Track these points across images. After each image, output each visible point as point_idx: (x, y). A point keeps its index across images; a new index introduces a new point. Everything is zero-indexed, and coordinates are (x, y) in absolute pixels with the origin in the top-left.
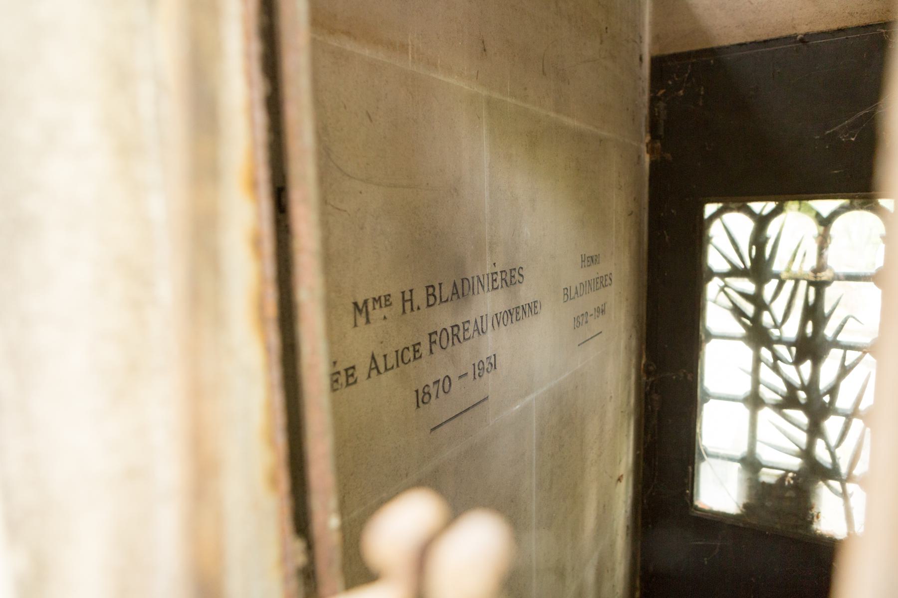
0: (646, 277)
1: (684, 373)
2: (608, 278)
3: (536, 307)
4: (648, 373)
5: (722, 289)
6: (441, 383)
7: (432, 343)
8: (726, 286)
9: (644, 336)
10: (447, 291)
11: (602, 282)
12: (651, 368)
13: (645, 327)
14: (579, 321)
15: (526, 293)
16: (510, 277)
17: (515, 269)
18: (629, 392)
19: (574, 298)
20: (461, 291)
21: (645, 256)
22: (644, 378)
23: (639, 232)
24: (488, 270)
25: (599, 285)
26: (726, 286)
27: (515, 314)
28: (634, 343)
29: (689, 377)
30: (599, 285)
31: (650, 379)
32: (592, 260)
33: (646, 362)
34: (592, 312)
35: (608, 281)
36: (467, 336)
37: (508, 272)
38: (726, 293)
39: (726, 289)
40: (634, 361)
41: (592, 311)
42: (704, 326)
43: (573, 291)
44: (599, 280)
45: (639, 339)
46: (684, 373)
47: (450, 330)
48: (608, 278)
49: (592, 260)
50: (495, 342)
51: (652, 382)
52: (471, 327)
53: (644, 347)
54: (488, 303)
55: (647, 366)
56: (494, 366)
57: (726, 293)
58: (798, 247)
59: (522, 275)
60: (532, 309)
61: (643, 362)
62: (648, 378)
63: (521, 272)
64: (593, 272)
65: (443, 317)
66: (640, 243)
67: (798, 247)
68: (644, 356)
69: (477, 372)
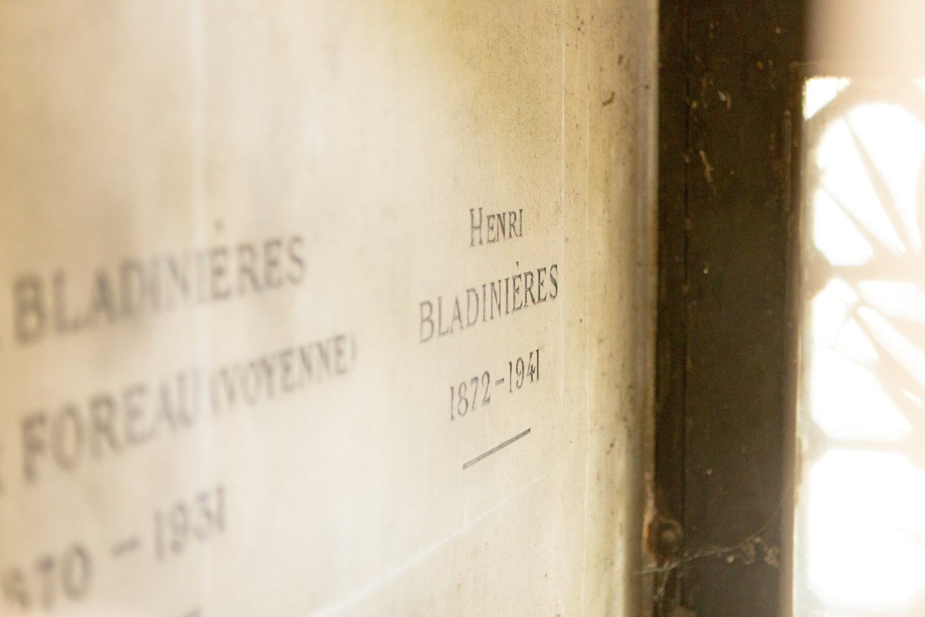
0: (652, 280)
1: (758, 547)
2: (545, 277)
3: (339, 352)
4: (661, 549)
5: (853, 313)
6: (480, 380)
7: (33, 447)
8: (862, 302)
9: (650, 445)
10: (78, 296)
11: (532, 288)
12: (669, 535)
13: (651, 422)
14: (467, 396)
15: (311, 312)
16: (268, 265)
17: (278, 243)
18: (609, 604)
19: (450, 331)
20: (118, 298)
21: (651, 219)
22: (652, 565)
23: (634, 153)
24: (202, 238)
25: (521, 297)
26: (862, 302)
27: (279, 369)
28: (621, 464)
29: (770, 559)
30: (521, 297)
31: (668, 566)
32: (505, 225)
33: (656, 518)
34: (504, 372)
35: (548, 287)
36: (140, 426)
37: (260, 249)
38: (860, 321)
39: (862, 312)
40: (621, 517)
41: (500, 370)
42: (813, 248)
43: (449, 310)
44: (520, 283)
45: (636, 455)
46: (758, 547)
47: (85, 413)
48: (545, 277)
49: (505, 225)
50: (222, 450)
51: (674, 572)
52: (150, 405)
53: (649, 476)
54: (196, 336)
55: (658, 529)
56: (217, 520)
57: (860, 321)
58: (859, 225)
59: (298, 261)
60: (331, 355)
61: (648, 518)
62: (660, 564)
63: (299, 251)
64: (504, 260)
65: (66, 373)
66: (634, 180)
67: (859, 225)
68: (650, 503)
69: (168, 536)
